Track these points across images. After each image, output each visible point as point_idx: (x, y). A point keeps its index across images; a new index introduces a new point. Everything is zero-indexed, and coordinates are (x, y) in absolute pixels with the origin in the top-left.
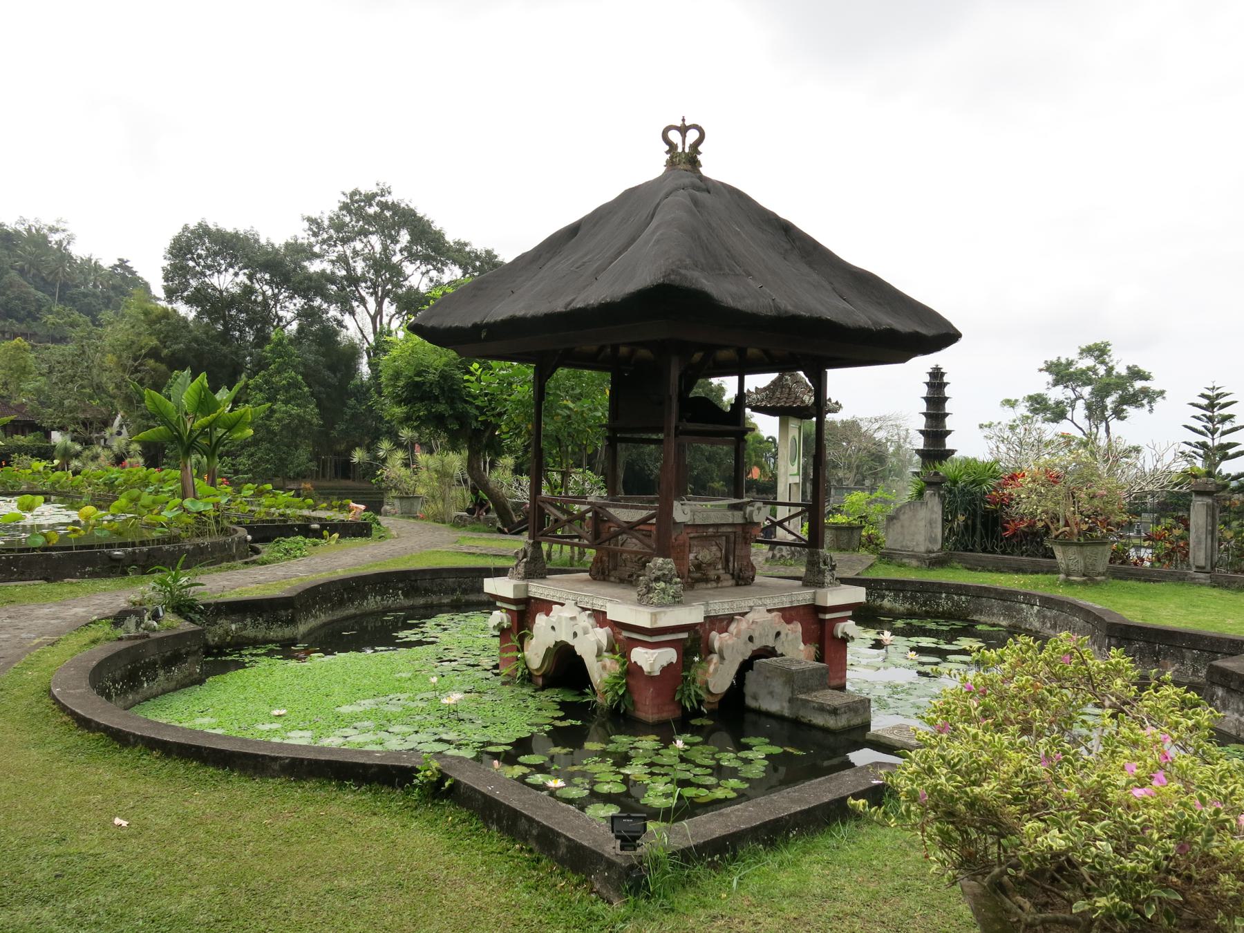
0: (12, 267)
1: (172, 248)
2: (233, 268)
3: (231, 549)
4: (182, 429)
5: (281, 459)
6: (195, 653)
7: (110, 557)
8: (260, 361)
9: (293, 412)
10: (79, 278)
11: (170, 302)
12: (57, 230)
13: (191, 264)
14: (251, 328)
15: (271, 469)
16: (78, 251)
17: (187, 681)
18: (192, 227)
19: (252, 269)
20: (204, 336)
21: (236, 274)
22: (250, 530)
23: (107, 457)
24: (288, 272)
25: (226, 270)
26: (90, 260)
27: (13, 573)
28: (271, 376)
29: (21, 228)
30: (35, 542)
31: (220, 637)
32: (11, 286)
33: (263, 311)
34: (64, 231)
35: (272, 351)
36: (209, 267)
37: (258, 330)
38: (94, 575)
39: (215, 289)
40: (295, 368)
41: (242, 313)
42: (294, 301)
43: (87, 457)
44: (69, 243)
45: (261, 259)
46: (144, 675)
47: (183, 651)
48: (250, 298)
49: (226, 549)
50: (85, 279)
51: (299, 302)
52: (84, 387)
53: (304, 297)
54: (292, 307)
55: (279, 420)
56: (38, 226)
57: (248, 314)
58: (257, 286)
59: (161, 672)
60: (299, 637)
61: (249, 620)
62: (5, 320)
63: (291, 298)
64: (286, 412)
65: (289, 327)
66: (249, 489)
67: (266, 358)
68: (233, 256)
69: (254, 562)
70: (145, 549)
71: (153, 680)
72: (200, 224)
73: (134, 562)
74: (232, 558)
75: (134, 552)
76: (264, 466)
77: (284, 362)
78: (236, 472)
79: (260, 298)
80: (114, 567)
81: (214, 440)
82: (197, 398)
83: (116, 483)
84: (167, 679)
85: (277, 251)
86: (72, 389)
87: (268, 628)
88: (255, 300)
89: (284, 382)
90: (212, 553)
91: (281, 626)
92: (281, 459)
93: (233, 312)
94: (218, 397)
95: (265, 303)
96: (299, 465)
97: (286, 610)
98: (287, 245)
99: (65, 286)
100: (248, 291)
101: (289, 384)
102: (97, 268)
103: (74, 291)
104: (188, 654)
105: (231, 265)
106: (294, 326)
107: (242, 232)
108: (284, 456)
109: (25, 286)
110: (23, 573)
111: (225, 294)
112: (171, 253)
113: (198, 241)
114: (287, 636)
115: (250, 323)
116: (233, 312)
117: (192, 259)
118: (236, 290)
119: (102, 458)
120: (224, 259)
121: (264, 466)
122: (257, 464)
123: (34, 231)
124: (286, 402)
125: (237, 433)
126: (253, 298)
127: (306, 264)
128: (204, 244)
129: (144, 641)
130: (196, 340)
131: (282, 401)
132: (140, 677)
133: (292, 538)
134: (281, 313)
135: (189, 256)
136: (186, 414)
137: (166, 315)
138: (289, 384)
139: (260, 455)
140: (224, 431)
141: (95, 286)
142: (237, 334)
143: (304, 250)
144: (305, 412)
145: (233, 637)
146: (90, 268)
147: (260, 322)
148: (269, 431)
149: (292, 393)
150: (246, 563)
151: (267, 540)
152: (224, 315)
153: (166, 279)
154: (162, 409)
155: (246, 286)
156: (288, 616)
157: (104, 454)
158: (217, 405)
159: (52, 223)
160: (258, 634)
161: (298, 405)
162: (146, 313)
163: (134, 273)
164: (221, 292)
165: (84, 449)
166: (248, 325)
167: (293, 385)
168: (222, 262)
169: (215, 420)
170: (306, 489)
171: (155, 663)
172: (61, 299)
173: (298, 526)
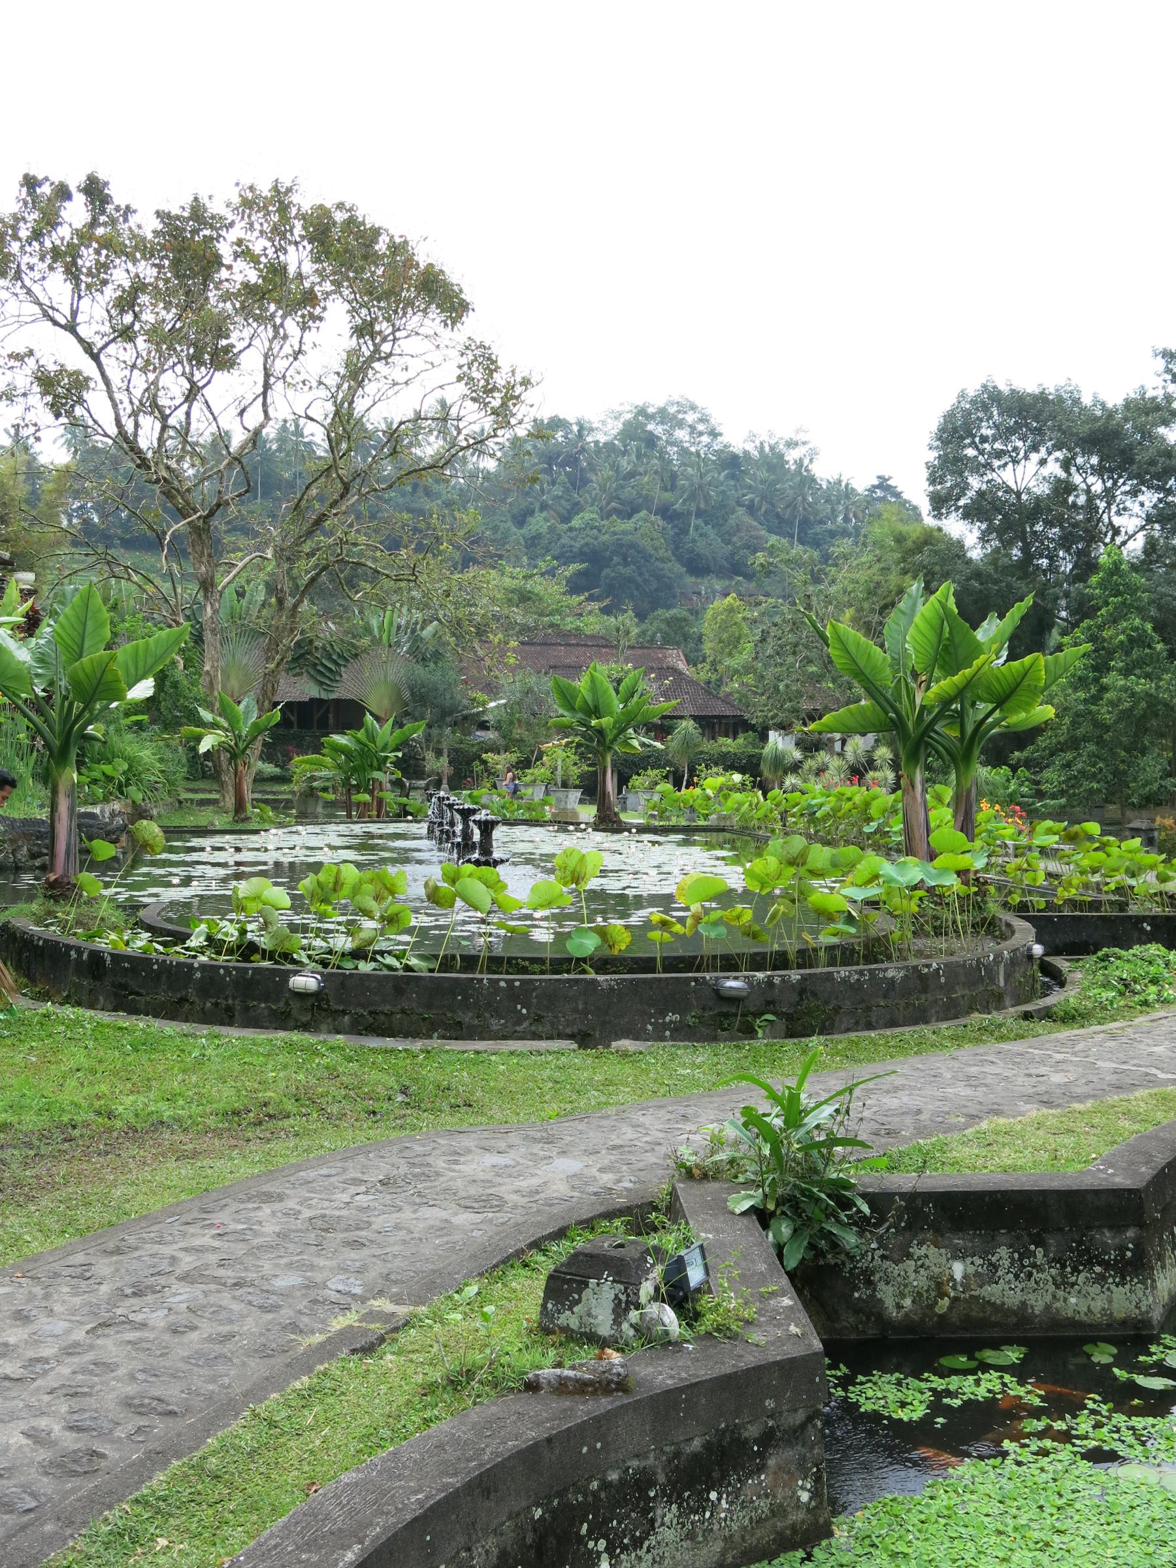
0: (739, 503)
1: (942, 430)
2: (1037, 451)
3: (992, 978)
4: (904, 706)
5: (1116, 773)
6: (796, 1435)
7: (717, 992)
8: (1081, 604)
9: (1138, 689)
10: (824, 509)
11: (938, 516)
12: (796, 444)
13: (971, 452)
14: (1068, 551)
15: (1099, 791)
16: (824, 471)
17: (764, 1535)
18: (971, 393)
19: (1069, 450)
20: (991, 570)
21: (1043, 462)
22: (1044, 926)
23: (839, 769)
24: (1131, 447)
25: (1026, 458)
26: (840, 481)
27: (521, 1019)
28: (1101, 627)
29: (750, 447)
30: (581, 945)
31: (918, 1296)
32: (738, 530)
33: (1089, 520)
34: (804, 443)
35: (1102, 585)
36: (999, 454)
37: (1079, 553)
38: (685, 1033)
39: (1008, 490)
40: (1141, 611)
41: (1052, 526)
42: (1141, 498)
43: (810, 770)
44: (811, 461)
45: (1084, 430)
46: (598, 1530)
47: (753, 1431)
48: (1066, 500)
49: (981, 979)
50: (833, 510)
51: (1149, 498)
52: (810, 661)
53: (1159, 489)
54: (1136, 508)
55: (1111, 703)
56: (772, 442)
57: (1062, 528)
58: (1077, 479)
59: (668, 1514)
60: (1157, 1315)
61: (1003, 1252)
62: (731, 578)
63: (1134, 493)
64: (1125, 689)
65: (1131, 545)
66: (1049, 831)
67: (1091, 598)
68: (1039, 431)
69: (1047, 1014)
70: (795, 975)
71: (637, 1543)
72: (985, 386)
73: (770, 1005)
74: (994, 1001)
75: (769, 983)
76: (1087, 785)
77: (1124, 603)
78: (1040, 795)
79: (1081, 501)
80: (726, 1015)
81: (970, 728)
82: (933, 638)
83: (818, 815)
84: (691, 1536)
85: (1110, 414)
86: (792, 665)
87: (1062, 1283)
88: (1074, 504)
89: (1122, 637)
90: (949, 988)
91: (1101, 1279)
92: (1116, 773)
93: (1039, 527)
94: (980, 635)
95: (1091, 506)
96: (1147, 783)
97: (1118, 1228)
98: (1128, 404)
99: (805, 523)
100: (1063, 488)
101: (1131, 640)
102: (849, 492)
103: (818, 529)
104: (768, 1439)
105: (1035, 448)
106: (1137, 545)
107: (1052, 390)
108: (1122, 767)
109: (756, 529)
110: (538, 1019)
111: (1024, 497)
112: (939, 439)
113: (981, 415)
114: (1119, 1315)
115: (1066, 542)
116: (1039, 527)
117: (973, 444)
118: (1044, 489)
119: (832, 771)
120: (1023, 439)
121: (1087, 785)
122: (1073, 781)
123: (767, 449)
124: (1126, 672)
125: (1015, 711)
126: (1071, 499)
127: (1162, 430)
128: (991, 417)
129: (605, 1404)
130: (978, 575)
131: (1120, 671)
132: (581, 1540)
133: (1137, 949)
134: (1117, 521)
135: (968, 441)
136: (915, 675)
137: (930, 539)
138: (1131, 640)
139: (1080, 766)
140: (990, 706)
141: (846, 519)
142: (1044, 562)
143: (1158, 408)
144: (1158, 687)
145: (955, 1300)
146: (841, 493)
147: (1082, 539)
148: (1097, 724)
149: (1136, 653)
150: (1027, 1016)
151: (1078, 949)
152: (1024, 532)
153: (932, 481)
154: (862, 663)
155: (1058, 480)
156: (1122, 1249)
157: (834, 763)
158: (976, 650)
159: (789, 434)
160: (1031, 1298)
161: (1147, 676)
162: (900, 539)
163: (898, 495)
164: (1018, 494)
165: (806, 757)
166: (1062, 546)
167: (1137, 640)
168: (1020, 444)
169: (969, 684)
170: (1164, 828)
171: (643, 1481)
172: (802, 541)
173: (1153, 920)
